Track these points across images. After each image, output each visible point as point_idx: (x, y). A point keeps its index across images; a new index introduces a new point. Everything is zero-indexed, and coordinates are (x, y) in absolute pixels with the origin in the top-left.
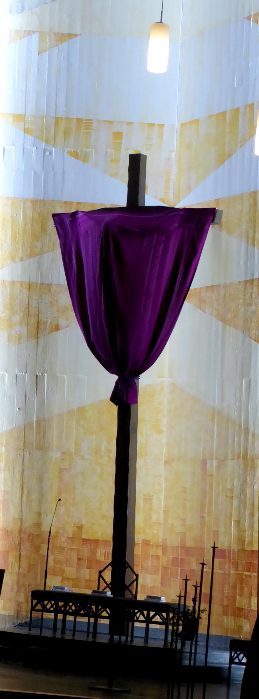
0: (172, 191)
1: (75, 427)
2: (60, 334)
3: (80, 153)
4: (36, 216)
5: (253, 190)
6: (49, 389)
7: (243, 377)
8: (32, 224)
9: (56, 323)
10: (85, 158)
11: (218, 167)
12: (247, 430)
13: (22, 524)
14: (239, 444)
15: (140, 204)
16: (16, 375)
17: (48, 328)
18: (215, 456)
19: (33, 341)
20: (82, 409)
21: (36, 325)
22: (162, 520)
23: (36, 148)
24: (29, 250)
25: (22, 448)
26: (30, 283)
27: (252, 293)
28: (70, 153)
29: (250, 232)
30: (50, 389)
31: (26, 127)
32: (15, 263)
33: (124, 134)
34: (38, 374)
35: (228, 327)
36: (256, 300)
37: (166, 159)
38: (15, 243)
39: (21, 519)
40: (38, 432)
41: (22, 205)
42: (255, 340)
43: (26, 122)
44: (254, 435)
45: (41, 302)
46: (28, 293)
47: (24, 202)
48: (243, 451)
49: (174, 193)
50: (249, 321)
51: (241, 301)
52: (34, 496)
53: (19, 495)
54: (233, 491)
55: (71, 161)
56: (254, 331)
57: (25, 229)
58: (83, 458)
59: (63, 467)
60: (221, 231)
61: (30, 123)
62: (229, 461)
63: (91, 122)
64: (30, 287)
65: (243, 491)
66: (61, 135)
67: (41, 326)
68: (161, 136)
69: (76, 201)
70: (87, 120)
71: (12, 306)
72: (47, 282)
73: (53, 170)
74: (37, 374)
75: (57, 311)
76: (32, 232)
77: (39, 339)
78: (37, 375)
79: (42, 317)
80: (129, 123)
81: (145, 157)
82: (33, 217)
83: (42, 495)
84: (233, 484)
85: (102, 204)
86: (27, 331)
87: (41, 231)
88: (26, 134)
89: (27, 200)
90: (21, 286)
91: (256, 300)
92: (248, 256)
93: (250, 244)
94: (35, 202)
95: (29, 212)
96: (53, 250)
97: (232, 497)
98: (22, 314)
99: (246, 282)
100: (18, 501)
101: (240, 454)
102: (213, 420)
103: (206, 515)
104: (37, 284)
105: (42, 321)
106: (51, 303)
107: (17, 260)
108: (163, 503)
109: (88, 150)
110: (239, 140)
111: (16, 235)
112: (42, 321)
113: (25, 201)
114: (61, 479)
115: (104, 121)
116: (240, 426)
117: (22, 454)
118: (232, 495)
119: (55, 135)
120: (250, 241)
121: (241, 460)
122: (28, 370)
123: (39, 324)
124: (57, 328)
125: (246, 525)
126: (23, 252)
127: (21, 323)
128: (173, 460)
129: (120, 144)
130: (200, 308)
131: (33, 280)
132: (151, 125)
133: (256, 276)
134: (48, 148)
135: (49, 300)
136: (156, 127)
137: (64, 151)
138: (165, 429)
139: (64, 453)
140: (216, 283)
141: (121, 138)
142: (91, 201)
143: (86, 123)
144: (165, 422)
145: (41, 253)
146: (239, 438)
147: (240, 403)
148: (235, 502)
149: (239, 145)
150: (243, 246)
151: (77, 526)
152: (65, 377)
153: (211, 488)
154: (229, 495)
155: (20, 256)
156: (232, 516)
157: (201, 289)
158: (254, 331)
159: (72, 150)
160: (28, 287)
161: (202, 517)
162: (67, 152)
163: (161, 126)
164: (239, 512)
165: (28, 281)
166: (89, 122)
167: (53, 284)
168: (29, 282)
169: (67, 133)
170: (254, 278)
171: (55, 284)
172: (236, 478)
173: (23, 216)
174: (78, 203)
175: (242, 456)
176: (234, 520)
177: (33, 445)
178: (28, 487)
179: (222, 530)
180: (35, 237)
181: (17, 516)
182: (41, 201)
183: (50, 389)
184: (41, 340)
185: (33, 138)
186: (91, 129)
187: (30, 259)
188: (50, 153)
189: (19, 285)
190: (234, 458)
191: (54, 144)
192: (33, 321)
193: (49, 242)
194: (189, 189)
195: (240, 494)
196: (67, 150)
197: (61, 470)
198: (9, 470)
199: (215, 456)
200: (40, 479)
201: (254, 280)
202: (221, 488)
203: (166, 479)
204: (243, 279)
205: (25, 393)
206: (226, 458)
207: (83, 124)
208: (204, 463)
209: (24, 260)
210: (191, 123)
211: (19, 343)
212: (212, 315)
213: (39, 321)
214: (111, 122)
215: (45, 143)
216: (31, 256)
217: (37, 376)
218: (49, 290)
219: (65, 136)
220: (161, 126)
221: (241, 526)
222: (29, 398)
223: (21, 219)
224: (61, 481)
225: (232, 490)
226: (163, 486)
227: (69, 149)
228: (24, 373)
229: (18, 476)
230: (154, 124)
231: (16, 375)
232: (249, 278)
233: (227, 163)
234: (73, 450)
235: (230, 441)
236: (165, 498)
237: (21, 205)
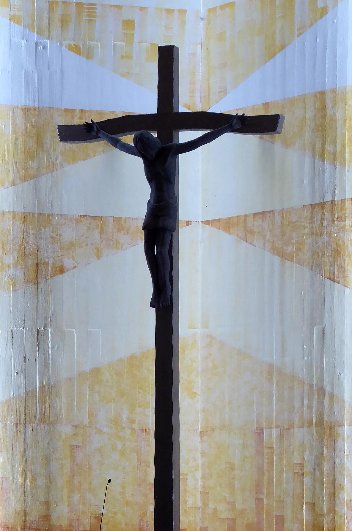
0: (199, 95)
1: (88, 393)
2: (65, 277)
3: (82, 46)
4: (30, 128)
5: (319, 89)
6: (54, 348)
7: (313, 325)
8: (25, 139)
9: (60, 264)
10: (89, 54)
11: (266, 63)
12: (321, 391)
13: (25, 517)
14: (310, 408)
15: (175, 111)
16: (12, 331)
17: (50, 270)
18: (274, 424)
19: (31, 288)
20: (96, 371)
21: (34, 267)
22: (199, 503)
23: (27, 41)
24: (22, 173)
25: (22, 422)
26: (25, 214)
27: (322, 219)
28: (70, 48)
29: (317, 142)
30: (56, 347)
31: (12, 13)
32: (5, 188)
33: (136, 24)
34: (40, 328)
35: (288, 263)
36: (329, 228)
37: (189, 54)
38: (4, 162)
39: (25, 510)
40: (43, 402)
41: (11, 114)
42: (330, 279)
43: (11, 7)
44: (332, 397)
45: (40, 238)
46: (22, 226)
47: (14, 110)
48: (316, 417)
49: (201, 97)
50: (320, 254)
51: (307, 231)
52: (41, 482)
53: (21, 481)
54: (303, 466)
55: (71, 58)
56: (328, 267)
57: (15, 145)
58: (100, 432)
59: (75, 443)
60: (273, 143)
61: (17, 8)
62: (296, 429)
63: (95, 7)
64: (25, 218)
65: (319, 465)
66: (57, 23)
67: (42, 268)
68: (183, 23)
69: (79, 107)
70: (89, 4)
71: (3, 244)
72: (46, 212)
73: (49, 69)
74: (39, 329)
75: (61, 249)
76: (24, 149)
77: (40, 285)
78: (38, 330)
79: (42, 256)
80: (142, 9)
81: (178, 49)
82: (26, 129)
83: (50, 480)
84: (304, 458)
85: (113, 112)
86: (23, 274)
87: (36, 147)
88: (12, 23)
89: (17, 107)
90: (14, 218)
91: (329, 228)
92: (315, 173)
93: (317, 158)
94: (27, 110)
95: (20, 122)
96: (53, 171)
97: (303, 474)
98: (16, 253)
99: (313, 206)
100: (20, 488)
101: (313, 420)
102: (271, 379)
103: (264, 497)
104: (33, 214)
105: (43, 261)
106: (53, 238)
107: (7, 184)
108: (200, 483)
109: (92, 43)
110: (296, 28)
111: (5, 152)
112: (43, 261)
113: (14, 108)
114: (73, 458)
115: (111, 6)
116: (311, 386)
117: (23, 430)
118: (302, 472)
119: (49, 24)
120: (317, 154)
121: (314, 428)
122: (28, 324)
123: (39, 265)
124: (62, 270)
125: (325, 508)
126: (14, 174)
127: (16, 265)
128: (213, 430)
129: (133, 35)
130: (247, 241)
131: (28, 210)
132: (170, 11)
133: (348, 196)
134: (42, 41)
135: (50, 235)
136: (176, 13)
137: (61, 44)
138: (199, 392)
139: (76, 426)
140: (268, 209)
141: (134, 28)
142: (98, 108)
143: (88, 8)
144: (199, 383)
145: (37, 176)
146: (311, 400)
147: (309, 358)
148: (307, 480)
149: (297, 33)
150: (308, 160)
151: (95, 516)
152: (73, 332)
153: (271, 463)
154: (297, 471)
155: (11, 178)
156: (303, 497)
157: (246, 216)
158: (328, 267)
159: (72, 43)
160: (23, 219)
161: (259, 500)
162: (65, 47)
163: (183, 12)
164: (314, 493)
165: (22, 211)
166: (92, 7)
167: (54, 214)
168: (24, 213)
169: (64, 21)
170: (325, 201)
171: (57, 214)
172: (307, 450)
173: (12, 128)
174: (82, 110)
175: (316, 422)
176: (305, 502)
177: (36, 417)
178: (31, 471)
179: (288, 514)
180: (29, 155)
181: (19, 508)
182: (34, 109)
183: (56, 347)
184: (42, 285)
185: (21, 28)
186: (95, 16)
187: (24, 183)
188: (44, 48)
189: (11, 217)
190: (303, 424)
191: (49, 36)
192: (31, 261)
193: (47, 160)
194: (224, 92)
195: (315, 470)
196: (65, 43)
197: (73, 448)
198: (7, 450)
199: (274, 424)
200: (47, 461)
201: (326, 203)
202: (285, 462)
203: (203, 454)
204: (308, 201)
205: (24, 352)
206: (291, 426)
207: (85, 10)
208: (259, 433)
209: (16, 185)
210: (222, 7)
211: (14, 290)
212: (264, 250)
213: (39, 261)
214: (119, 7)
215: (37, 34)
216: (24, 179)
217: (38, 331)
218: (50, 222)
219: (62, 24)
220: (183, 12)
221: (317, 509)
222: (29, 360)
223: (11, 132)
224: (74, 462)
225: (302, 466)
226: (200, 462)
227: (68, 42)
228: (21, 329)
229: (19, 457)
230: (174, 10)
231: (12, 331)
232: (318, 200)
233: (279, 56)
234: (87, 422)
235: (297, 404)
236: (203, 477)
237: (10, 115)
